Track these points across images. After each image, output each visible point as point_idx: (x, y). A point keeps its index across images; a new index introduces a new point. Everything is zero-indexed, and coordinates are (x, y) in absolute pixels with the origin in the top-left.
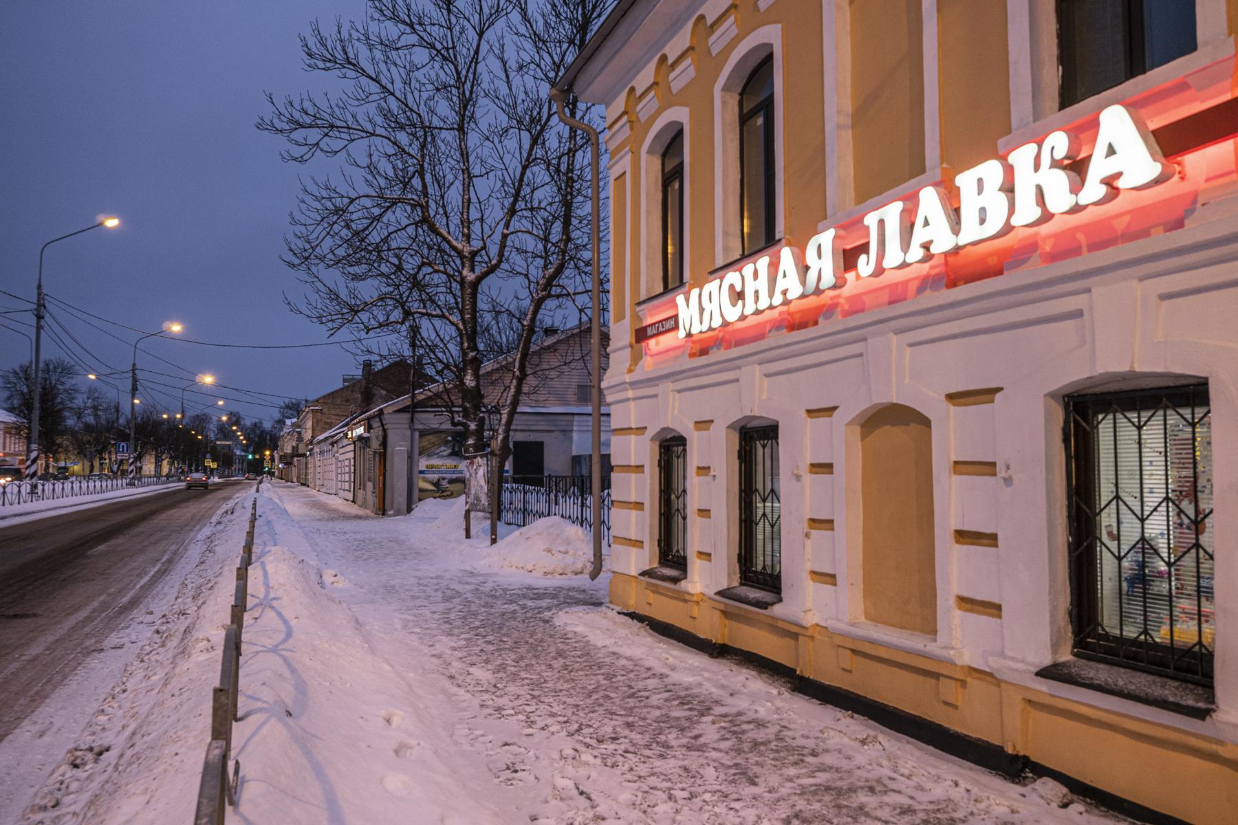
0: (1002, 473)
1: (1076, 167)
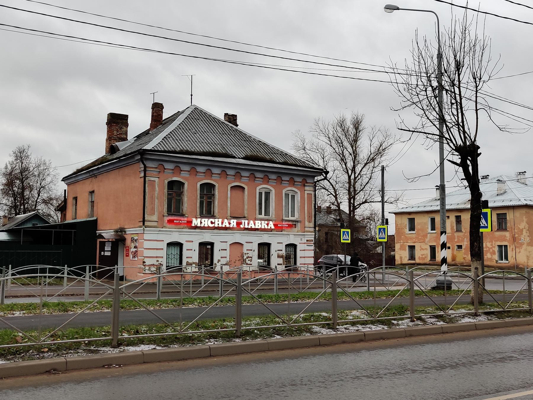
0: (193, 250)
1: (268, 224)
